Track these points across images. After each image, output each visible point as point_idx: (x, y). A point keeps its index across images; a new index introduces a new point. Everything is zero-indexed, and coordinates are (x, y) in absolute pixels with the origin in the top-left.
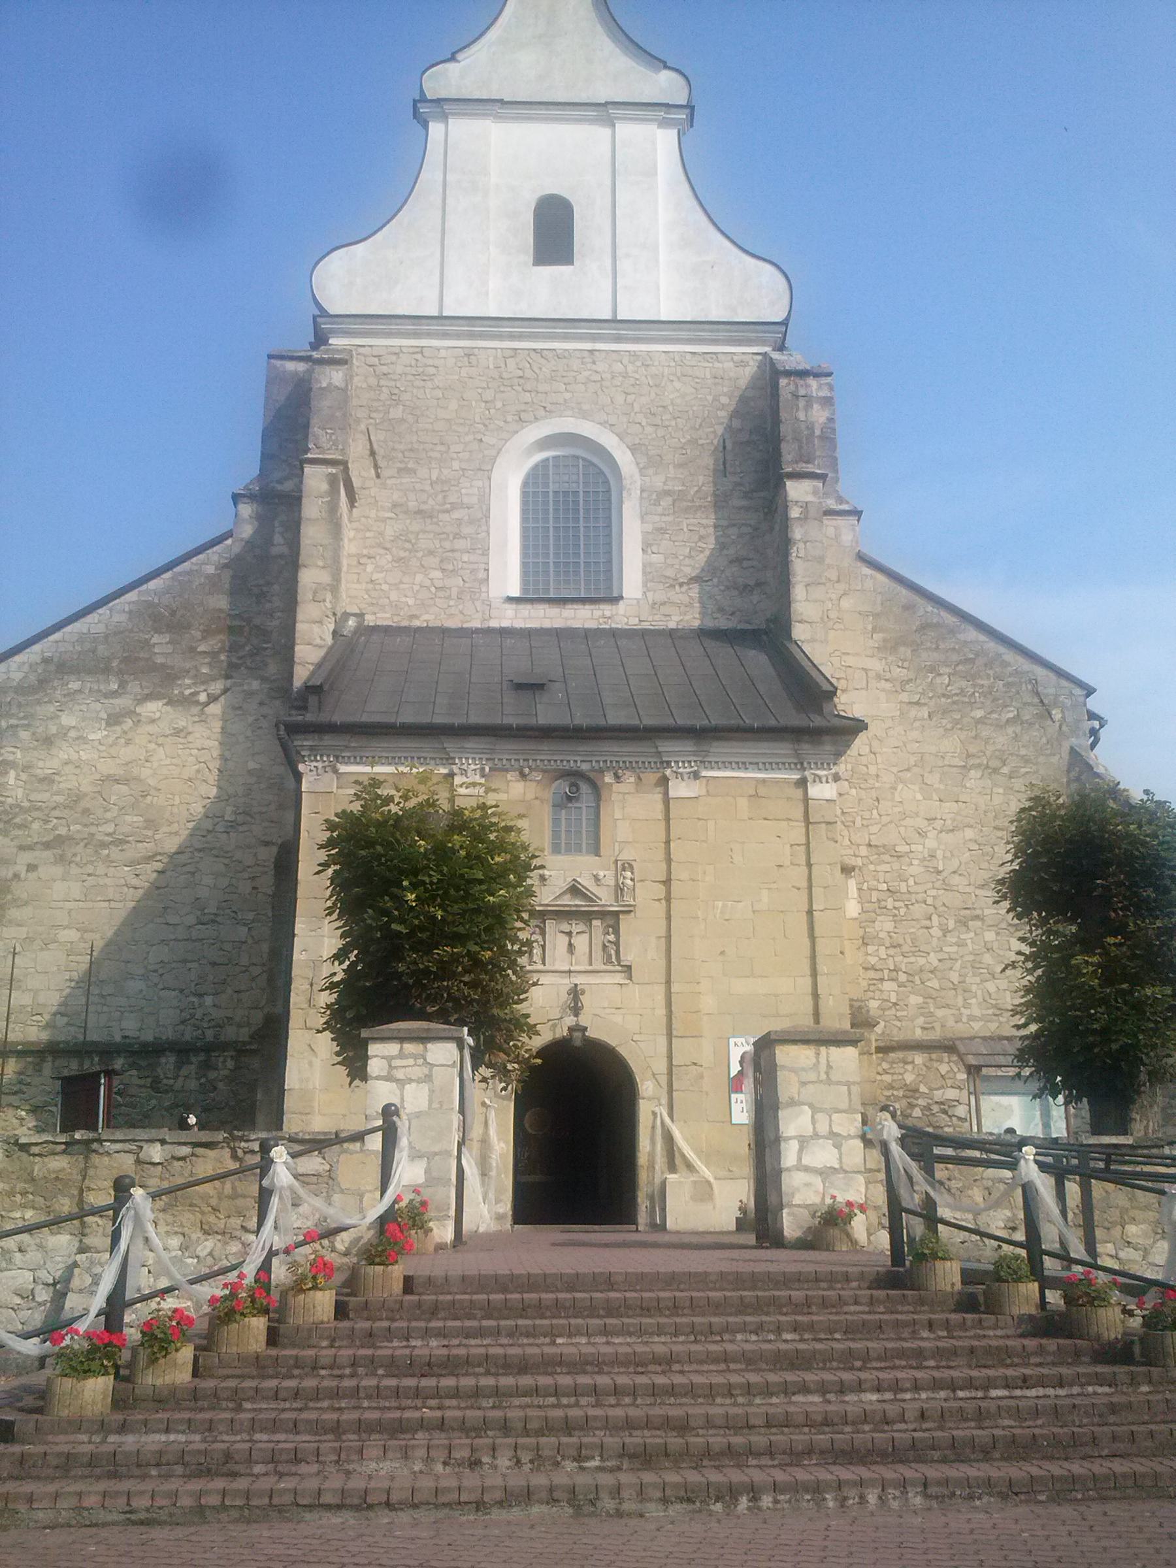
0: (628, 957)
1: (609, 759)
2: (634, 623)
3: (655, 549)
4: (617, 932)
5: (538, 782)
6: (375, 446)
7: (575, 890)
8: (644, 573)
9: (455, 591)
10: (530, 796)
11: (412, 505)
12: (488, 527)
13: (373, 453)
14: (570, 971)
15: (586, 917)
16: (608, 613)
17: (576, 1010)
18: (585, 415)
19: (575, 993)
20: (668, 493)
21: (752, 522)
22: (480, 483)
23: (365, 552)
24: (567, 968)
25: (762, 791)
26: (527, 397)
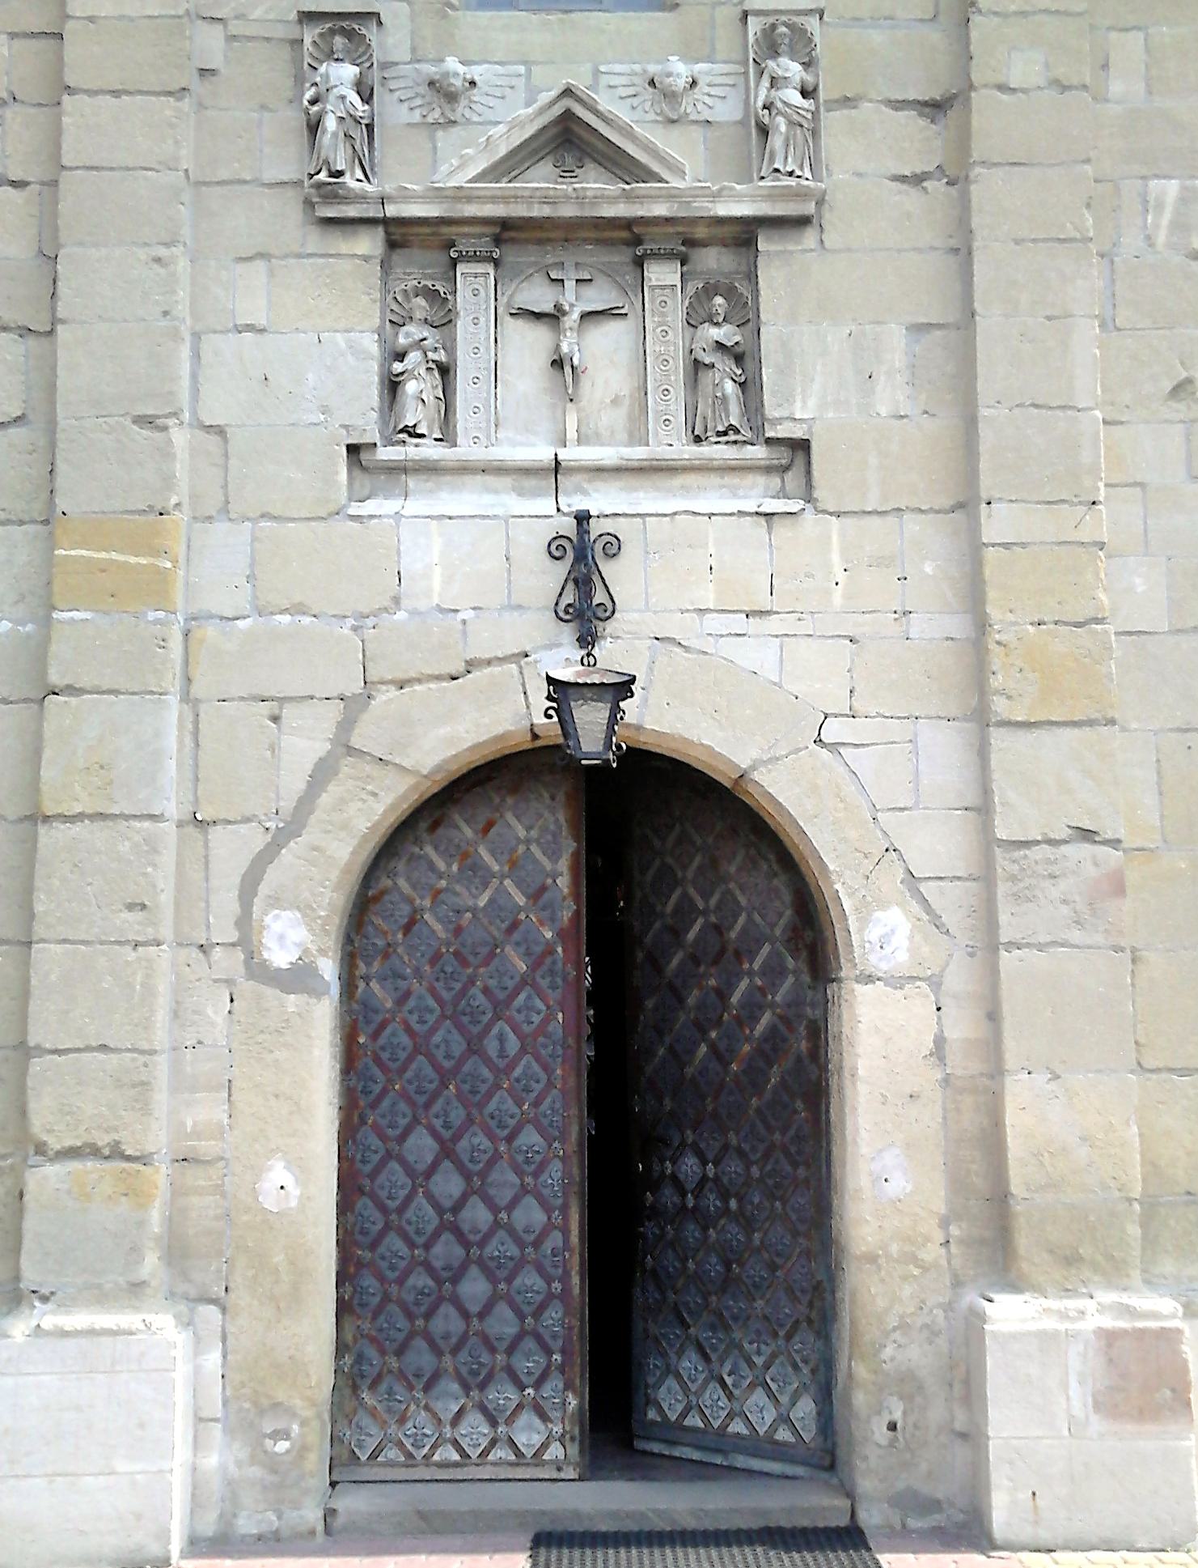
0: (794, 406)
7: (569, 137)
15: (632, 242)
17: (585, 612)
19: (582, 554)
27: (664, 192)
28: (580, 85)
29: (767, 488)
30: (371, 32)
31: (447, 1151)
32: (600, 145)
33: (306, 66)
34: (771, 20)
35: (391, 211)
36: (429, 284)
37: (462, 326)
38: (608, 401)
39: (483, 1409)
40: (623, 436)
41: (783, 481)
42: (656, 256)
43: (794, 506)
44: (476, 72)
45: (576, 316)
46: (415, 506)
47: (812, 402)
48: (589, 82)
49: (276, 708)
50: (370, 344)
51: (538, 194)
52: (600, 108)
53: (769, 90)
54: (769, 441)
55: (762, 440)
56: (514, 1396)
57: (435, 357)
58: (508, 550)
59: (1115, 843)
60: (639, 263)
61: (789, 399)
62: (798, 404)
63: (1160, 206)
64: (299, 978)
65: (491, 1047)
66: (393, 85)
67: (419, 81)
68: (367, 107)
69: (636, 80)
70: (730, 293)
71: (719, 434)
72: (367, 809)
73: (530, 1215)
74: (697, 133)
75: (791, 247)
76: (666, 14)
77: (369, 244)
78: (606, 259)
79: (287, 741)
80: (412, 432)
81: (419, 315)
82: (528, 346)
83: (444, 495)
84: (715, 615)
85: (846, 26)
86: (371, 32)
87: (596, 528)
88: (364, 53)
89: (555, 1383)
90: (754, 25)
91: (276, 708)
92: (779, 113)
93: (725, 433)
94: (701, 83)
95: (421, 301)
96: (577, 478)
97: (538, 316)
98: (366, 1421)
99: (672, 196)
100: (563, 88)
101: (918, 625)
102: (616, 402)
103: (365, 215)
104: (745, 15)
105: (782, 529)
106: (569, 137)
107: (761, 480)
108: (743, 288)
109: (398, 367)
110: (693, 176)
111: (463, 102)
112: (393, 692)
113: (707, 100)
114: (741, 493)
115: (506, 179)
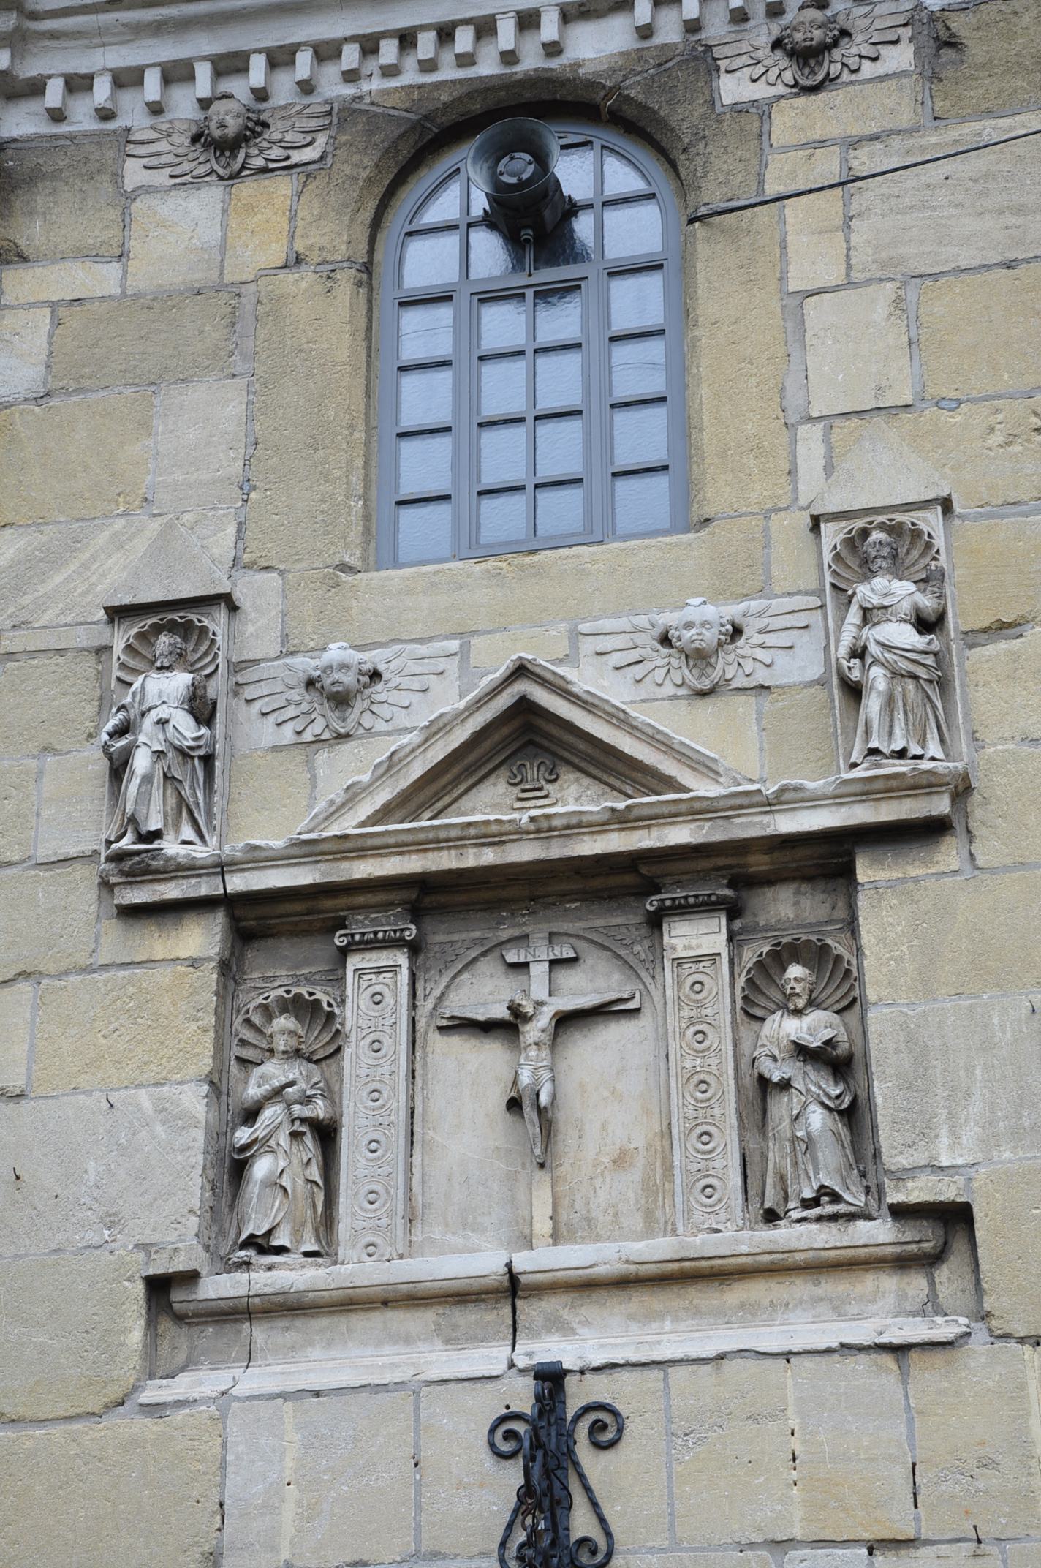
7: (526, 735)
15: (635, 889)
27: (683, 807)
28: (541, 659)
29: (902, 1296)
30: (217, 622)
32: (581, 745)
33: (113, 683)
34: (860, 523)
35: (237, 883)
36: (303, 991)
37: (355, 1057)
38: (606, 1160)
40: (637, 1222)
41: (932, 1283)
43: (943, 1329)
44: (372, 658)
45: (544, 1020)
47: (969, 1135)
48: (562, 649)
50: (194, 1100)
51: (472, 832)
52: (575, 690)
53: (860, 628)
54: (900, 1212)
55: (885, 1210)
57: (307, 1112)
58: (417, 1446)
60: (655, 922)
61: (926, 1134)
62: (944, 1141)
66: (249, 693)
67: (292, 682)
68: (204, 730)
69: (640, 639)
70: (818, 956)
71: (807, 1204)
74: (745, 706)
75: (915, 871)
76: (691, 536)
77: (202, 938)
78: (599, 922)
80: (261, 1245)
81: (281, 1044)
82: (470, 1079)
83: (316, 1353)
84: (807, 1552)
85: (989, 516)
86: (217, 622)
87: (577, 1395)
88: (206, 653)
90: (832, 535)
92: (876, 661)
93: (815, 1202)
94: (747, 631)
95: (284, 1022)
96: (550, 1304)
99: (699, 810)
100: (512, 666)
102: (621, 1160)
103: (193, 894)
104: (816, 522)
106: (526, 735)
107: (889, 1283)
108: (838, 946)
109: (243, 1135)
111: (360, 704)
113: (759, 654)
114: (853, 1309)
115: (428, 814)
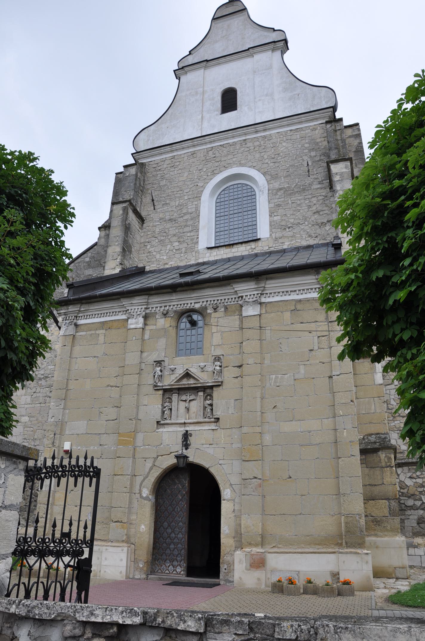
0: (218, 413)
1: (209, 299)
2: (266, 249)
3: (275, 214)
4: (212, 398)
5: (172, 317)
6: (154, 198)
7: (187, 375)
8: (270, 225)
9: (184, 250)
10: (167, 325)
11: (167, 218)
12: (199, 220)
13: (153, 200)
14: (185, 423)
15: (195, 390)
16: (253, 247)
17: (186, 446)
18: (241, 165)
19: (186, 436)
20: (281, 189)
21: (324, 194)
22: (196, 203)
23: (147, 240)
24: (183, 421)
25: (299, 307)
26: (217, 164)
30: (163, 363)
31: (169, 526)
35: (164, 388)
39: (172, 565)
42: (200, 391)
46: (165, 430)
49: (145, 459)
50: (160, 406)
56: (176, 563)
59: (260, 479)
63: (272, 379)
64: (147, 498)
65: (176, 509)
72: (156, 474)
73: (180, 536)
77: (161, 392)
79: (147, 464)
80: (166, 419)
82: (182, 405)
86: (163, 363)
89: (182, 562)
91: (145, 459)
97: (184, 401)
98: (156, 566)
101: (234, 446)
105: (215, 431)
110: (205, 379)
112: (161, 457)
